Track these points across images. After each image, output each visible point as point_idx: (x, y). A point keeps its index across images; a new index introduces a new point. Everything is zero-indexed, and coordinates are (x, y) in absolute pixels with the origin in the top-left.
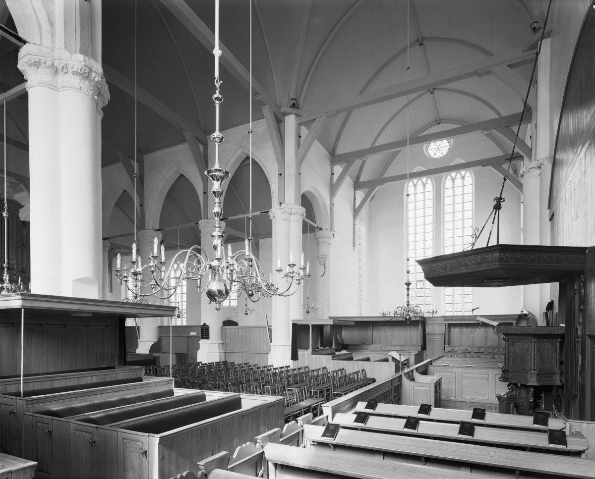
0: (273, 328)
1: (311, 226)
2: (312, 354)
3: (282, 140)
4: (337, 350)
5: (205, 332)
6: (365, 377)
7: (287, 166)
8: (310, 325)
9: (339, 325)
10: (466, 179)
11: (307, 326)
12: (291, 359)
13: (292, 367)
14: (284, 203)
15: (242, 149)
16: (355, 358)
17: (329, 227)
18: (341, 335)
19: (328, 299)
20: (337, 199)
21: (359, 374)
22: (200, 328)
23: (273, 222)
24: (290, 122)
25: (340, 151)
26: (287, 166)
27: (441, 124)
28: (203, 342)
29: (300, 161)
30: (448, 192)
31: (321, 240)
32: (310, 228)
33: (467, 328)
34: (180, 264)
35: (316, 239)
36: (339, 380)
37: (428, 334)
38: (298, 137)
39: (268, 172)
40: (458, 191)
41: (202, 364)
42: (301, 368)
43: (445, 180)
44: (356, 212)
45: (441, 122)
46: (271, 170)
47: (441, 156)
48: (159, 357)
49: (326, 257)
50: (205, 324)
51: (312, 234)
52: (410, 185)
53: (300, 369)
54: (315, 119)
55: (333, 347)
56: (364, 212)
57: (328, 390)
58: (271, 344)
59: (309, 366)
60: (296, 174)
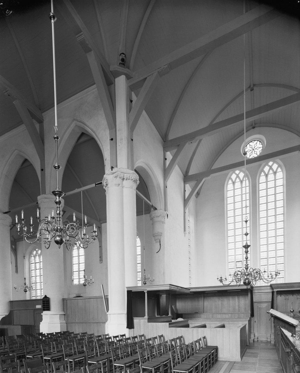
0: (109, 297)
1: (146, 203)
2: (148, 322)
3: (112, 101)
4: (173, 319)
5: (46, 303)
6: (206, 345)
7: (118, 130)
8: (146, 292)
9: (175, 294)
10: (277, 174)
11: (142, 293)
12: (127, 328)
13: (127, 336)
14: (117, 167)
15: (75, 122)
16: (190, 326)
17: (162, 207)
18: (176, 306)
19: (164, 273)
20: (170, 183)
21: (200, 342)
22: (42, 301)
23: (107, 191)
24: (121, 83)
25: (171, 137)
26: (118, 130)
27: (256, 128)
28: (45, 314)
29: (132, 127)
30: (262, 186)
31: (156, 219)
32: (145, 207)
33: (293, 296)
34: (38, 251)
35: (152, 219)
36: (180, 352)
37: (256, 302)
38: (129, 102)
39: (100, 141)
40: (271, 184)
41: (74, 335)
42: (136, 337)
43: (260, 176)
44: (186, 202)
45: (256, 125)
46: (103, 138)
47: (256, 156)
48: (7, 329)
49: (161, 234)
50: (46, 296)
51: (148, 215)
52: (229, 183)
53: (134, 338)
54: (146, 78)
55: (170, 315)
56: (191, 203)
57: (166, 365)
58: (107, 313)
59: (145, 334)
60: (128, 141)
